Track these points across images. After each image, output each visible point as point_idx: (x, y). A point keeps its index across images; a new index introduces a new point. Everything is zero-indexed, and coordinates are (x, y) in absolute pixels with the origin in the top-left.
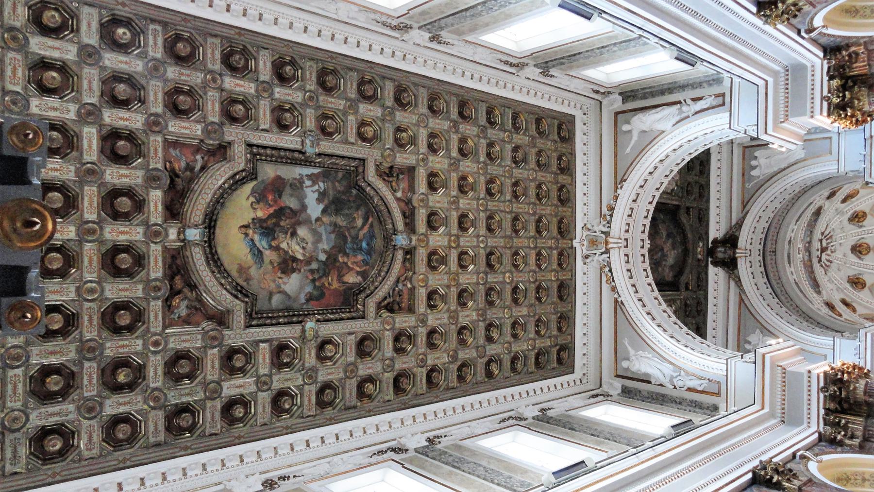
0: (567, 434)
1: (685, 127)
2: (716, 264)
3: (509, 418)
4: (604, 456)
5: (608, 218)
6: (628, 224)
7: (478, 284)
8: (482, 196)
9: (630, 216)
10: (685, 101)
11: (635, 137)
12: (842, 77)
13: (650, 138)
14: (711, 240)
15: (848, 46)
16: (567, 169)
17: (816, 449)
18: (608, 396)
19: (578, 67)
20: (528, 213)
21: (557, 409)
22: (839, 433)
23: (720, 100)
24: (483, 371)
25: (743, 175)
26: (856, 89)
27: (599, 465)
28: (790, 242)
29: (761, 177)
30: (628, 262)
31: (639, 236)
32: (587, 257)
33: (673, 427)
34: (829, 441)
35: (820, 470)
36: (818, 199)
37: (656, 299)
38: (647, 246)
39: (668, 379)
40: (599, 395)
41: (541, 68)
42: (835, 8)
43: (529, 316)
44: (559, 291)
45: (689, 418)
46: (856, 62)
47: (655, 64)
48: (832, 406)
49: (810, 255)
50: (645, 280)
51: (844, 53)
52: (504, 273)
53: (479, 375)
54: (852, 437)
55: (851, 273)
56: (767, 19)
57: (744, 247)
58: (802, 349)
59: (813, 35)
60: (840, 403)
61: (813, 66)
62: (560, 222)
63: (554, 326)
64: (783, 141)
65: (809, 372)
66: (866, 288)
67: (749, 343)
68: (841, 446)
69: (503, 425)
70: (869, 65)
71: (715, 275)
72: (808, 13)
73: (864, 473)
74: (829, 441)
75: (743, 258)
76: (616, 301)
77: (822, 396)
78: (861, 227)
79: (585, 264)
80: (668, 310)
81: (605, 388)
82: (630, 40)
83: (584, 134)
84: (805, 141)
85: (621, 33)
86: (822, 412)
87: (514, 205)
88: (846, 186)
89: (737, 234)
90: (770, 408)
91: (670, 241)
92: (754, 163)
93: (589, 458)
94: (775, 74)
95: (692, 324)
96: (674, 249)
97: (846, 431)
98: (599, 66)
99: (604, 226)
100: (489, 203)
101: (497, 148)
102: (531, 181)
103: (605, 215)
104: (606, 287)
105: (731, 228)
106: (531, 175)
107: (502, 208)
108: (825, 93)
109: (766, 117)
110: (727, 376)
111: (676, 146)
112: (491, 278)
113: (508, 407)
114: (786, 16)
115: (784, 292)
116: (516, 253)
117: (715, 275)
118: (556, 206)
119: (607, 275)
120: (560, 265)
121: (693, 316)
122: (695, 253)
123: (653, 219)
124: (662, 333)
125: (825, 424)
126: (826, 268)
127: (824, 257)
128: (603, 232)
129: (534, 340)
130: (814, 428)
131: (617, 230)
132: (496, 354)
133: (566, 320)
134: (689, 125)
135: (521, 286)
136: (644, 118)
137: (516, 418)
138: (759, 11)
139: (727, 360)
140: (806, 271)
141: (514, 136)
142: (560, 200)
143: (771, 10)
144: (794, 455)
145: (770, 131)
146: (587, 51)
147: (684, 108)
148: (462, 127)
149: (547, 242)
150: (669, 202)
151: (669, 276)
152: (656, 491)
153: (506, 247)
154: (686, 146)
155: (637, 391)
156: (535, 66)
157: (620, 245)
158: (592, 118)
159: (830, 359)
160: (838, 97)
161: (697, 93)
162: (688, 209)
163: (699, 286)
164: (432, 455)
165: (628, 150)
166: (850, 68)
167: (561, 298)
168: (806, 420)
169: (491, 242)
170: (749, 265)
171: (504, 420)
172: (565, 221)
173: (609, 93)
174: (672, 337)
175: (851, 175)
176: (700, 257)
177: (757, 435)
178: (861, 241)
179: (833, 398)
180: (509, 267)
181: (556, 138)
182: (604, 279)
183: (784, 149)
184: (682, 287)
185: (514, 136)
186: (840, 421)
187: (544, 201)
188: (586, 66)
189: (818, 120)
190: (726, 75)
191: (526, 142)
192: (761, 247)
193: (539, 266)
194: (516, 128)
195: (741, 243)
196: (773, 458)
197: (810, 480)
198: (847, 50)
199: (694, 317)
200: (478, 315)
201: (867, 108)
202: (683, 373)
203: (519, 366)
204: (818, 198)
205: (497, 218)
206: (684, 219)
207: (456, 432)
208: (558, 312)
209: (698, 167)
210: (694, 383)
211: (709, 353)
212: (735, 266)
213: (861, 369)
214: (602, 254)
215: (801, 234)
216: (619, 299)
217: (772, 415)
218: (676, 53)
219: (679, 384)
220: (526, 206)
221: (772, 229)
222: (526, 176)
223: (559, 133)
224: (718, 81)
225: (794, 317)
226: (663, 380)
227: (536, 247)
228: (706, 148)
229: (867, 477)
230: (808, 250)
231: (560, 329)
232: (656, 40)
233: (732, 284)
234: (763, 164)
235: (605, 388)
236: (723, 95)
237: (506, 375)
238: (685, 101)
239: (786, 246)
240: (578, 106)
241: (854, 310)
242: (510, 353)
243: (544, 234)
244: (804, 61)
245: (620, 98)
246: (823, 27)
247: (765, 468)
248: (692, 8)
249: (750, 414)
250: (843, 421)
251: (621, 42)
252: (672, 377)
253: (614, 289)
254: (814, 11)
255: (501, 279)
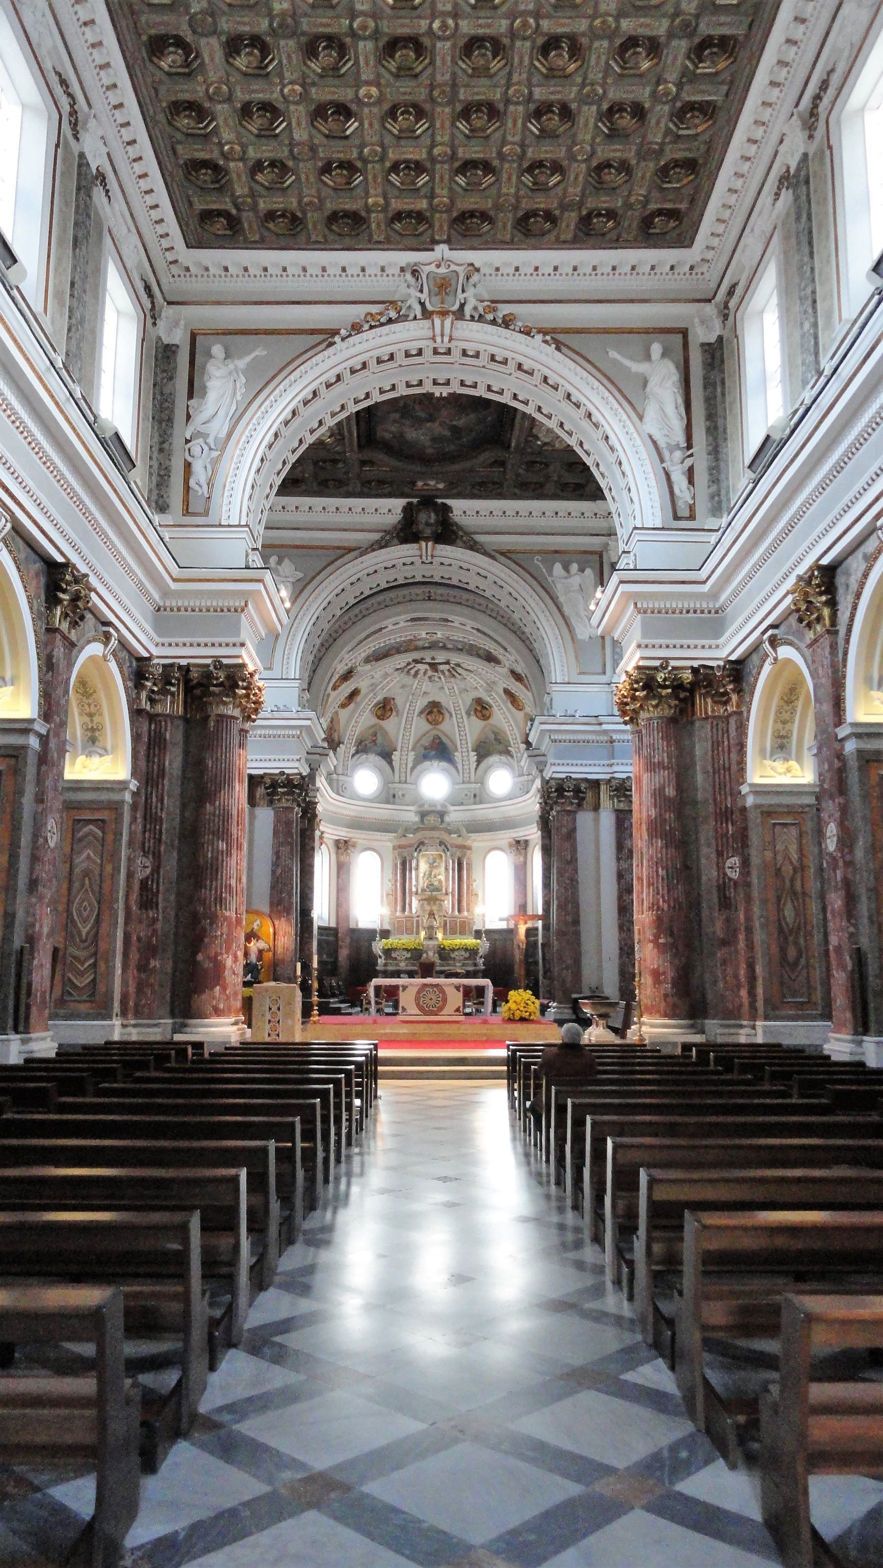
0: (64, 230)
1: (644, 455)
2: (408, 510)
3: (69, 95)
4: (38, 308)
5: (490, 317)
6: (477, 355)
7: (353, 14)
8: (545, 24)
9: (493, 358)
10: (691, 455)
11: (637, 367)
12: (693, 688)
13: (631, 394)
14: (449, 502)
15: (739, 691)
16: (590, 231)
17: (124, 654)
18: (153, 317)
19: (786, 253)
20: (504, 142)
21: (110, 211)
22: (155, 684)
23: (684, 512)
24: (162, 30)
25: (556, 552)
26: (674, 703)
27: (15, 293)
28: (447, 620)
29: (550, 579)
30: (408, 355)
31: (456, 375)
32: (415, 273)
33: (117, 435)
34: (139, 671)
35: (92, 658)
36: (512, 658)
37: (343, 407)
38: (438, 391)
39: (202, 429)
40: (152, 300)
41: (798, 169)
42: (801, 674)
43: (292, 145)
44: (347, 214)
45: (138, 463)
46: (715, 702)
47: (764, 400)
48: (194, 675)
49: (424, 648)
50: (374, 387)
51: (730, 687)
52: (378, 85)
53: (157, 18)
54: (152, 701)
55: (399, 702)
56: (807, 580)
57: (436, 553)
58: (277, 637)
59: (767, 646)
60: (199, 684)
61: (717, 646)
62: (484, 216)
63: (277, 203)
64: (605, 606)
65: (243, 645)
66: (377, 721)
67: (279, 562)
68: (136, 687)
69: (54, 80)
70: (707, 718)
71: (389, 510)
72: (801, 637)
73: (101, 715)
74: (139, 671)
75: (418, 553)
76: (335, 332)
77: (209, 661)
78: (468, 714)
79: (402, 270)
80: (323, 429)
81: (168, 312)
82: (816, 354)
83: (653, 268)
84: (603, 638)
85: (832, 337)
86: (183, 662)
87: (521, 108)
88: (529, 694)
89: (459, 542)
90: (176, 591)
91: (447, 433)
92: (574, 567)
93: (24, 273)
94: (714, 595)
95: (303, 472)
96: (434, 439)
97: (158, 693)
98: (780, 298)
99: (475, 308)
100: (528, 44)
101: (646, 65)
102: (569, 149)
103: (495, 310)
104: (360, 311)
105: (467, 534)
106: (581, 150)
107: (515, 78)
108: (673, 663)
109: (646, 582)
110: (220, 526)
111: (613, 440)
112: (366, 47)
113: (96, 95)
114: (804, 607)
115: (365, 612)
116: (420, 113)
117: (389, 510)
118: (516, 208)
119: (381, 314)
120: (398, 216)
121: (314, 472)
122: (423, 476)
123: (488, 402)
124: (281, 418)
125: (164, 666)
126: (406, 670)
127: (422, 667)
128: (462, 306)
129: (229, 99)
130: (155, 651)
131: (466, 334)
132: (202, 64)
133: (288, 229)
134: (647, 462)
135: (352, 126)
136: (669, 384)
137: (73, 113)
138: (821, 568)
139: (247, 526)
140: (400, 644)
141: (666, 108)
142: (527, 216)
143: (818, 586)
144: (108, 624)
145: (623, 588)
146: (812, 269)
147: (678, 455)
148: (681, 46)
149: (446, 190)
150: (516, 432)
151: (387, 430)
152: (4, 416)
153: (432, 87)
154: (612, 458)
155: (171, 375)
156: (805, 155)
157: (439, 339)
158: (680, 283)
159: (267, 674)
160: (665, 680)
161: (702, 476)
162: (502, 464)
163: (369, 482)
164: (78, 188)
165: (613, 354)
166: (706, 695)
167: (333, 217)
168: (166, 640)
169: (443, 47)
170: (408, 560)
171: (63, 82)
172: (486, 227)
173: (726, 317)
174: (276, 435)
175: (546, 699)
176: (420, 484)
177: (130, 572)
178: (447, 715)
179: (207, 675)
180: (392, 96)
181: (653, 206)
182: (374, 309)
183: (592, 607)
184: (367, 455)
185: (666, 108)
186: (173, 685)
187: (527, 179)
188: (785, 273)
189: (633, 654)
190: (724, 521)
191: (650, 137)
192: (437, 579)
193: (395, 168)
194: (685, 111)
195: (445, 550)
196: (97, 593)
197: (73, 645)
198: (733, 690)
199: (315, 475)
200: (283, 14)
201: (643, 715)
202: (215, 454)
203: (184, 122)
204: (512, 658)
205: (495, 65)
206: (487, 456)
207: (117, 208)
208: (304, 213)
209: (573, 478)
210: (200, 474)
211: (255, 497)
212: (405, 540)
213: (256, 711)
214: (422, 304)
215: (458, 636)
216: (337, 339)
217: (166, 593)
218: (776, 436)
219: (196, 446)
220: (517, 138)
221: (465, 596)
222: (580, 137)
223: (660, 212)
224: (717, 510)
225: (327, 626)
226: (199, 419)
227: (432, 159)
228: (606, 492)
229: (96, 719)
230: (433, 646)
231: (271, 215)
232: (808, 402)
233: (377, 536)
234: (568, 581)
235: (168, 312)
236: (692, 517)
237: (163, 90)
238: (691, 455)
239: (437, 615)
240: (710, 255)
241: (343, 706)
242: (210, 99)
243: (461, 180)
244: (727, 634)
245: (712, 339)
246: (776, 659)
247: (77, 581)
248: (851, 464)
249: (162, 562)
250: (173, 689)
251: (816, 338)
252: (205, 436)
253: (356, 328)
254: (803, 646)
255: (364, 77)
